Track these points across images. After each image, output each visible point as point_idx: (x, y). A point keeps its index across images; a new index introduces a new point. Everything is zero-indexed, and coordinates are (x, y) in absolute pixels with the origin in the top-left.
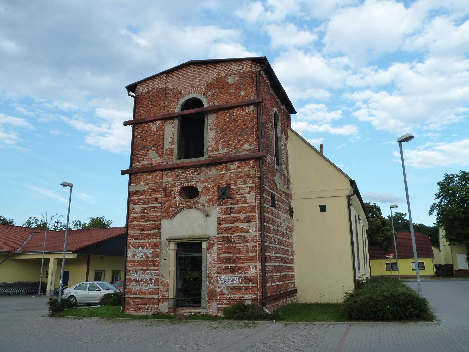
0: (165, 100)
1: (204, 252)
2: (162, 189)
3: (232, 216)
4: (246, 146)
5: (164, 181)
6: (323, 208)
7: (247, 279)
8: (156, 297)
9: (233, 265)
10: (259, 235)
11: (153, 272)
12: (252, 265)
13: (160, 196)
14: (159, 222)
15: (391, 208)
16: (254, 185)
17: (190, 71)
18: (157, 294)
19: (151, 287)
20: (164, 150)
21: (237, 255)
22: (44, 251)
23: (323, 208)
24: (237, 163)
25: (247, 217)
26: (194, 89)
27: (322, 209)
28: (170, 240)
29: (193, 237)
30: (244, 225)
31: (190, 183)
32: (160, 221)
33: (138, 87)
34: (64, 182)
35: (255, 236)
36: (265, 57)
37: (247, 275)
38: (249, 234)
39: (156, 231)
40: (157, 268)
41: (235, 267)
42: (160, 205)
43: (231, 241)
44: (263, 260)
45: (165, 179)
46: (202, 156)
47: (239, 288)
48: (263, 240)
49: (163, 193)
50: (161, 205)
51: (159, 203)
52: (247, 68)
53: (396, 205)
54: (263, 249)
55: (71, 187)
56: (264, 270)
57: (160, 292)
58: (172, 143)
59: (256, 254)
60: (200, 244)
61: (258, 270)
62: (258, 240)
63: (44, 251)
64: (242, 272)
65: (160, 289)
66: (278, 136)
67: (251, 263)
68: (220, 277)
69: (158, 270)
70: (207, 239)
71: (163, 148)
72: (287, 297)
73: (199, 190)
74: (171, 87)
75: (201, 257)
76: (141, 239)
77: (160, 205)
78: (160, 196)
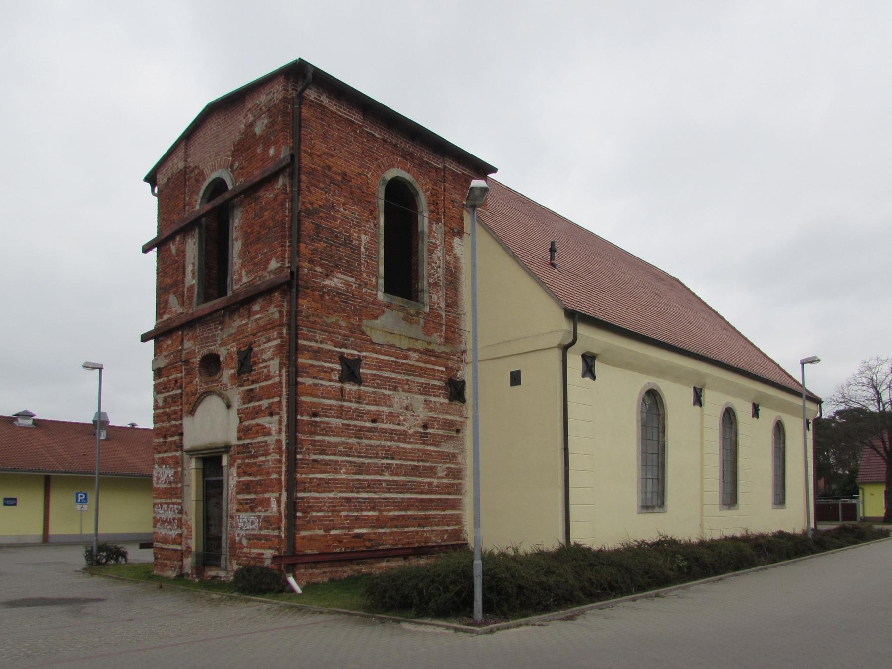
0: (185, 193)
1: (225, 471)
2: (181, 361)
3: (253, 405)
4: (273, 265)
5: (186, 346)
6: (516, 379)
7: (267, 522)
8: (179, 547)
9: (252, 496)
10: (286, 440)
11: (176, 506)
12: (272, 496)
13: (179, 375)
14: (180, 422)
15: (803, 364)
16: (278, 341)
17: (212, 127)
18: (180, 544)
19: (174, 533)
20: (186, 290)
21: (258, 478)
22: (96, 472)
23: (516, 379)
24: (260, 300)
25: (270, 406)
26: (219, 160)
27: (515, 379)
28: (192, 452)
29: (213, 446)
30: (264, 421)
31: (211, 348)
32: (181, 419)
33: (158, 176)
34: (87, 363)
35: (279, 441)
36: (300, 59)
37: (268, 514)
38: (271, 438)
39: (176, 438)
40: (179, 501)
41: (255, 499)
42: (179, 391)
43: (251, 452)
44: (293, 485)
45: (188, 344)
46: (225, 294)
47: (258, 538)
48: (294, 445)
49: (185, 369)
50: (182, 391)
51: (178, 389)
52: (277, 92)
53: (815, 357)
54: (293, 465)
55: (100, 369)
56: (293, 505)
57: (184, 540)
58: (193, 277)
59: (280, 475)
60: (220, 458)
61: (283, 506)
62: (284, 448)
63: (96, 472)
64: (263, 510)
65: (184, 536)
66: (419, 230)
67: (272, 492)
68: (239, 516)
69: (180, 504)
70: (227, 448)
71: (184, 287)
72: (410, 557)
73: (221, 359)
74: (192, 165)
75: (221, 481)
76: (165, 451)
77: (179, 391)
78: (179, 375)
